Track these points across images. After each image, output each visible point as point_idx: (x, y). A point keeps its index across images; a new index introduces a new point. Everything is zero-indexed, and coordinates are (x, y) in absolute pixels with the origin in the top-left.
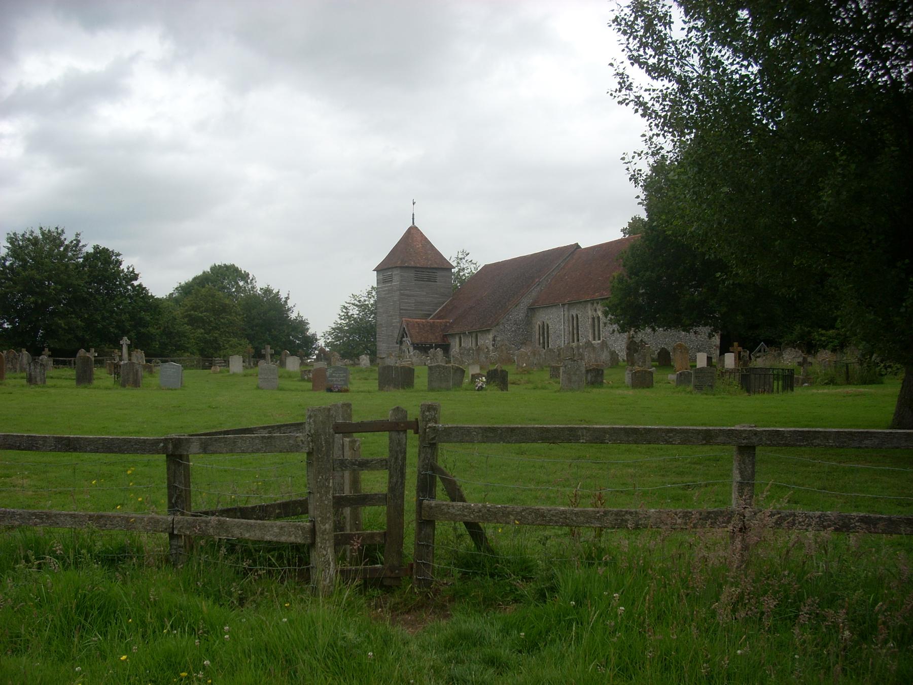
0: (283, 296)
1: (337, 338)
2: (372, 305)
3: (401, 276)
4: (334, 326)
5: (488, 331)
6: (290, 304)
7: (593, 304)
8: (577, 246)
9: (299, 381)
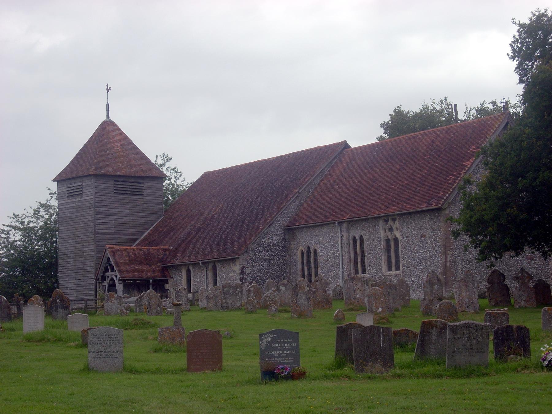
2: (41, 228)
3: (96, 187)
5: (233, 260)
7: (386, 221)
8: (345, 145)
9: (77, 346)
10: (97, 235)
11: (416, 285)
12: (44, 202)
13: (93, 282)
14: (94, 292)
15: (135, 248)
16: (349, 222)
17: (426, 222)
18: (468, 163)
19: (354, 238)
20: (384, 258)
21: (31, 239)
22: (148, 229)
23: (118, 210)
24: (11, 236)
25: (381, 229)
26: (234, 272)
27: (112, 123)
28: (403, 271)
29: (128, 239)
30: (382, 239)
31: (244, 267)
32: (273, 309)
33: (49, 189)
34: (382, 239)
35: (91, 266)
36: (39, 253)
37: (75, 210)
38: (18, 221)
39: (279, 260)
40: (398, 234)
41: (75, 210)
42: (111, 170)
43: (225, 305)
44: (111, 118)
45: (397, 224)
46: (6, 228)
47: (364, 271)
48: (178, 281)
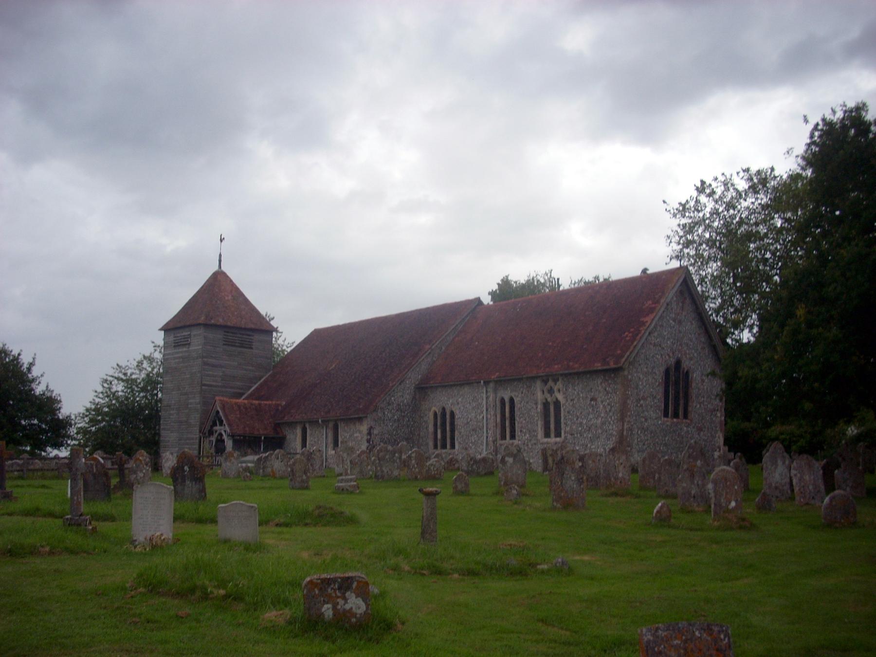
0: (25, 360)
1: (93, 421)
2: (143, 380)
3: (205, 338)
4: (89, 405)
5: (360, 420)
6: (35, 372)
7: (545, 382)
12: (147, 354)
14: (197, 446)
15: (246, 401)
16: (496, 382)
17: (598, 384)
18: (648, 319)
19: (503, 401)
20: (540, 424)
21: (133, 390)
24: (114, 387)
25: (538, 389)
26: (360, 432)
27: (224, 274)
30: (539, 402)
32: (515, 492)
34: (539, 402)
35: (195, 419)
36: (139, 405)
38: (121, 372)
40: (560, 397)
42: (221, 320)
43: (379, 473)
44: (223, 268)
45: (560, 384)
46: (110, 379)
47: (513, 437)
48: (294, 439)
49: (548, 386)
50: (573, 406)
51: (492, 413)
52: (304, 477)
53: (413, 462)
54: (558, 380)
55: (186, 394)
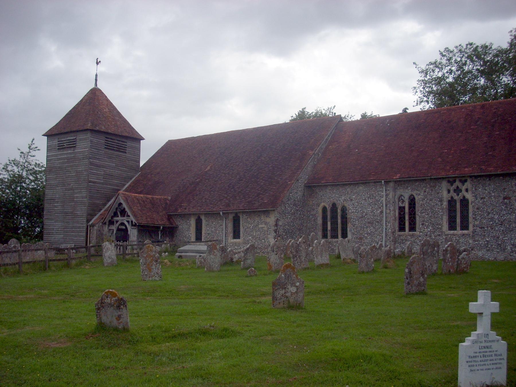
5: (266, 213)
10: (90, 184)
11: (492, 245)
13: (85, 225)
14: (84, 234)
16: (396, 182)
20: (445, 218)
22: (128, 182)
23: (107, 163)
28: (474, 231)
29: (113, 189)
31: (278, 219)
33: (19, 149)
37: (66, 160)
39: (300, 214)
40: (469, 196)
41: (66, 160)
42: (103, 127)
44: (99, 86)
45: (468, 184)
49: (454, 186)
50: (484, 203)
51: (392, 209)
52: (422, 279)
53: (449, 255)
54: (466, 181)
55: (72, 189)
